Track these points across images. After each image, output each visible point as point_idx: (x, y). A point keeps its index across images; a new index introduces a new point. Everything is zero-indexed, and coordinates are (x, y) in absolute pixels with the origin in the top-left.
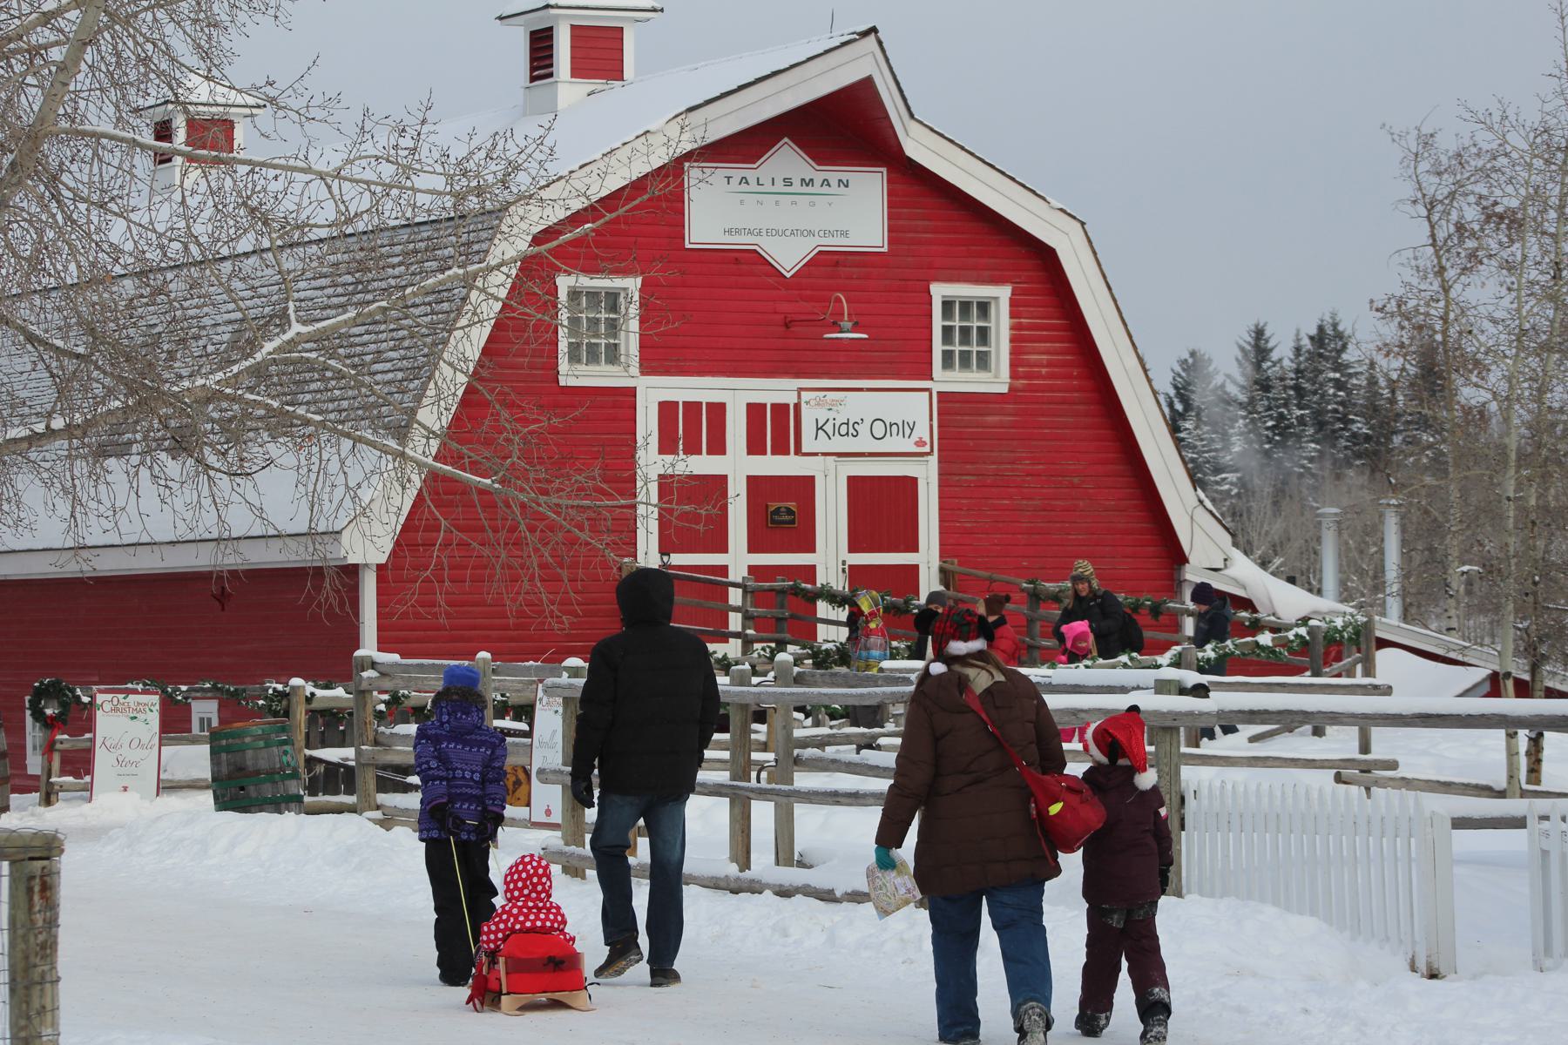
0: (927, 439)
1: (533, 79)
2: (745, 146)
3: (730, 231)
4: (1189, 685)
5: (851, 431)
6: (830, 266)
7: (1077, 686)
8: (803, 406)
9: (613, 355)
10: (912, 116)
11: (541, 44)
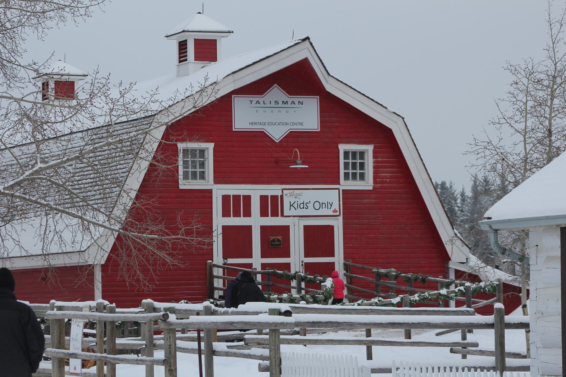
0: (338, 210)
1: (180, 62)
2: (257, 88)
3: (252, 124)
4: (283, 311)
5: (305, 206)
6: (295, 138)
7: (246, 312)
8: (284, 196)
9: (202, 176)
10: (329, 74)
11: (183, 46)
